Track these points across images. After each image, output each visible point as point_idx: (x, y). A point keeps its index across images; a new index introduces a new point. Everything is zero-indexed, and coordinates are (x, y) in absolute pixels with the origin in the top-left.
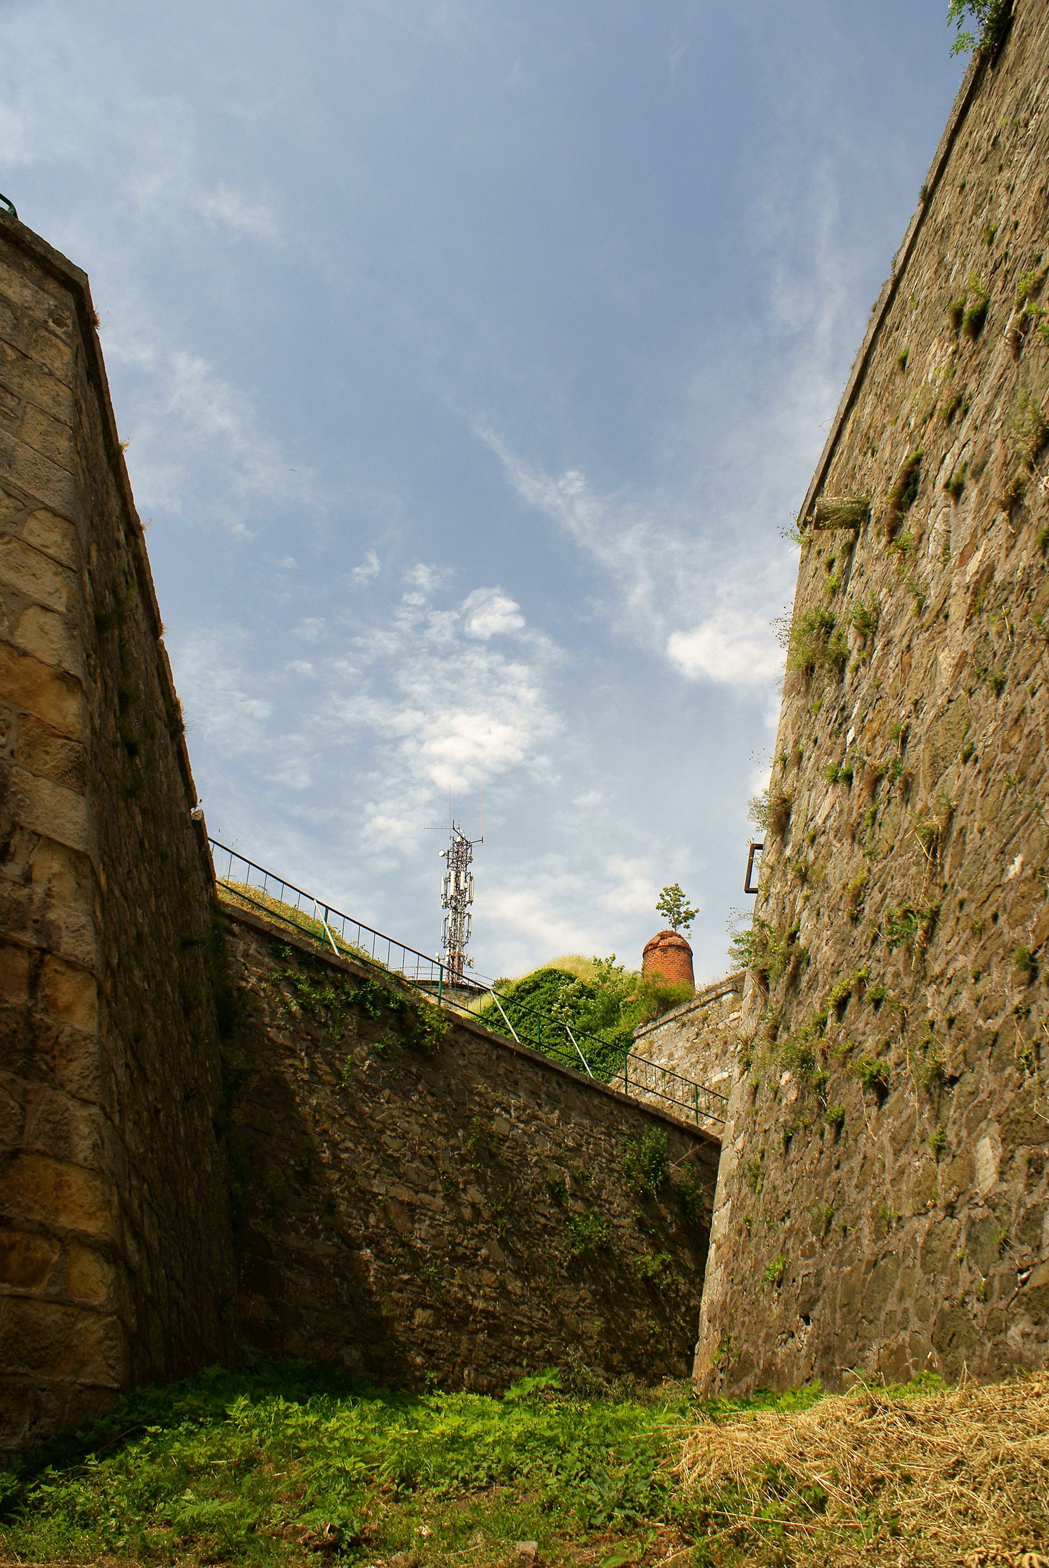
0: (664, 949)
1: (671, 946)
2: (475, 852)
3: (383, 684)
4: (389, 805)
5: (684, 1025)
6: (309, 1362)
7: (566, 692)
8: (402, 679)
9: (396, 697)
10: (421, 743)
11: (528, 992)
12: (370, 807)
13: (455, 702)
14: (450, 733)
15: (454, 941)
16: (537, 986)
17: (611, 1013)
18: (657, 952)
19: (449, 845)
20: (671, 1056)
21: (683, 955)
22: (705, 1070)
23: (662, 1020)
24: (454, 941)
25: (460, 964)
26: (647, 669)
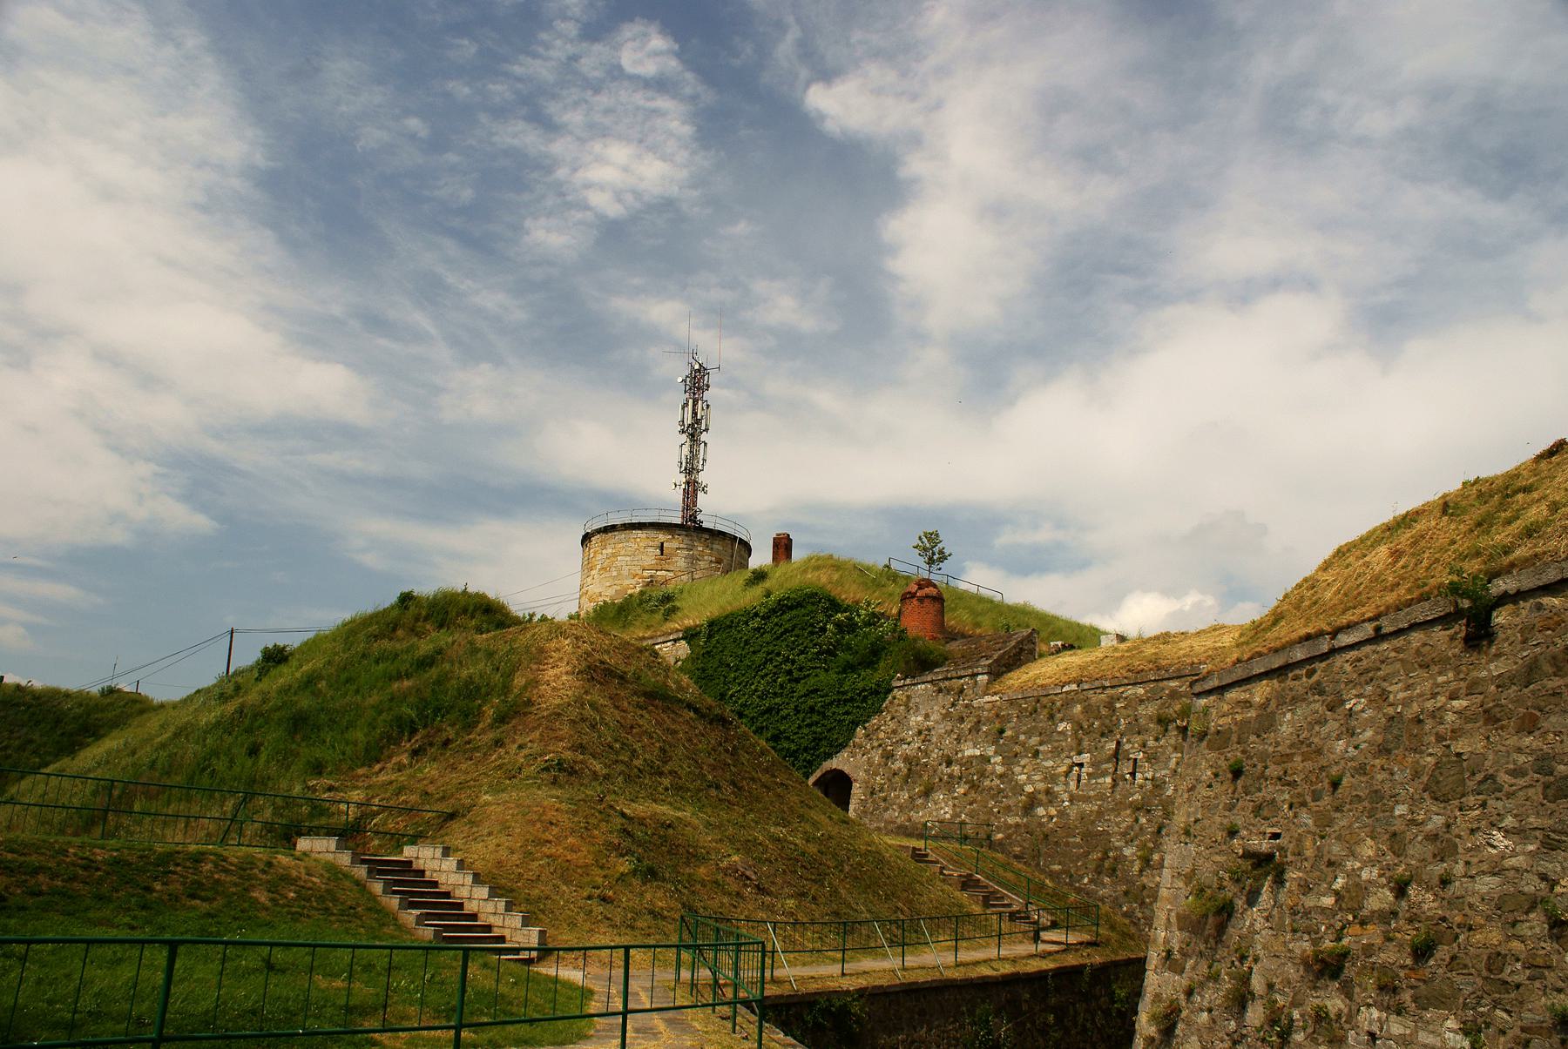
0: (921, 600)
1: (927, 596)
2: (713, 378)
3: (533, 106)
4: (543, 221)
5: (940, 691)
6: (688, 870)
7: (713, 128)
8: (552, 108)
9: (550, 127)
10: (575, 170)
11: (791, 608)
12: (528, 223)
13: (603, 133)
14: (601, 160)
15: (692, 489)
16: (799, 605)
17: (875, 654)
18: (915, 602)
19: (688, 372)
20: (927, 716)
21: (937, 605)
22: (958, 740)
23: (919, 679)
24: (692, 489)
25: (695, 491)
26: (794, 129)
